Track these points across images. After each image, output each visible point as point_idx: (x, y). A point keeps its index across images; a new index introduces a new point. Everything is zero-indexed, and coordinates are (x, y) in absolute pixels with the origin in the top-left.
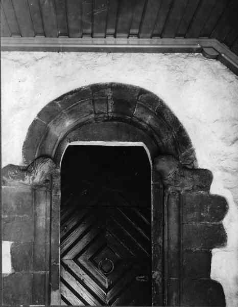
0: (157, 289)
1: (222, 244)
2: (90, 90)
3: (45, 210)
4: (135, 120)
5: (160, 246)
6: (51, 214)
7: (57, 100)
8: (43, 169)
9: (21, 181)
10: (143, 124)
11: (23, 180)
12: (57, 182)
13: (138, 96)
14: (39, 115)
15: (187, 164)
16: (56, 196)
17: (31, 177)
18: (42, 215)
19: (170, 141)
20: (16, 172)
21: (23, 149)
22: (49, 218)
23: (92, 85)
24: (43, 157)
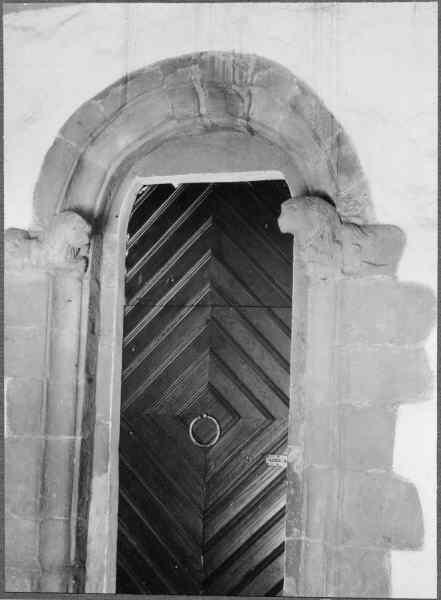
1: (420, 396)
2: (160, 72)
7: (96, 98)
10: (271, 134)
14: (63, 131)
17: (44, 252)
19: (322, 167)
23: (164, 61)
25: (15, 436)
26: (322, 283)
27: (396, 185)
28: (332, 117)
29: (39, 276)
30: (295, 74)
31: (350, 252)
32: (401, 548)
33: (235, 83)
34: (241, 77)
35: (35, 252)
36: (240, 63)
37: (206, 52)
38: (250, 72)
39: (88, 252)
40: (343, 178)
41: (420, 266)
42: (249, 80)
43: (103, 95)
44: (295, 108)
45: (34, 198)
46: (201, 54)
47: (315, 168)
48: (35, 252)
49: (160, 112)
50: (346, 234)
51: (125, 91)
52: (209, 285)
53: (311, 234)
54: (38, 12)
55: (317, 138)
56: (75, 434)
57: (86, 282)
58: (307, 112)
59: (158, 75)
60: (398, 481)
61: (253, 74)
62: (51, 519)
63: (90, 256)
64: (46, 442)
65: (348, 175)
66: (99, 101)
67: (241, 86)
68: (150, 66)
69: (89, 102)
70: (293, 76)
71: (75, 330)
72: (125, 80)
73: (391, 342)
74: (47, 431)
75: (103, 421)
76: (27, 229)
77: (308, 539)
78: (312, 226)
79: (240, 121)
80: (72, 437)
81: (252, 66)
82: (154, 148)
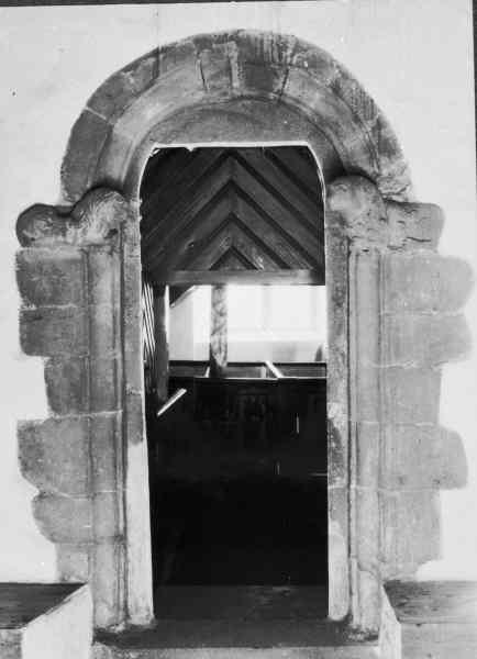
0: (338, 440)
3: (110, 292)
4: (288, 101)
5: (343, 355)
6: (122, 293)
7: (126, 69)
8: (104, 212)
9: (60, 238)
10: (304, 109)
11: (64, 235)
12: (134, 230)
13: (292, 56)
14: (91, 103)
15: (394, 194)
16: (131, 256)
17: (80, 231)
18: (106, 301)
20: (50, 220)
21: (62, 172)
22: (118, 306)
24: (104, 186)
26: (364, 254)
27: (433, 154)
28: (372, 101)
30: (335, 58)
31: (396, 229)
32: (448, 487)
33: (273, 61)
34: (280, 57)
35: (71, 231)
36: (280, 45)
37: (242, 30)
38: (289, 52)
40: (384, 160)
41: (458, 240)
42: (289, 60)
43: (133, 67)
44: (336, 89)
46: (238, 31)
47: (352, 143)
48: (71, 231)
49: (190, 86)
50: (394, 214)
51: (157, 64)
52: (254, 250)
53: (359, 212)
55: (357, 119)
58: (346, 94)
59: (191, 50)
60: (443, 432)
61: (292, 56)
62: (100, 493)
65: (389, 157)
66: (129, 73)
67: (279, 65)
68: (183, 40)
69: (119, 73)
70: (332, 60)
72: (156, 53)
73: (435, 309)
75: (134, 391)
77: (358, 488)
78: (359, 206)
79: (272, 96)
81: (291, 46)
82: (184, 119)
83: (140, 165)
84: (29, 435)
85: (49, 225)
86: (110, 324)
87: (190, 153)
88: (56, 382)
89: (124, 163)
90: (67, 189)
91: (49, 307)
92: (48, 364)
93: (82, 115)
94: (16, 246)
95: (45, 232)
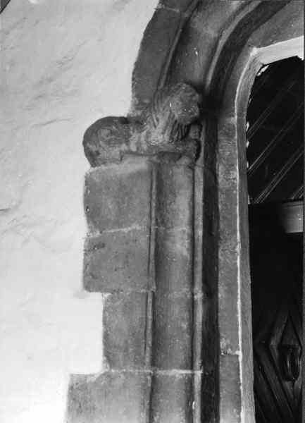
9: (124, 147)
17: (144, 133)
25: (113, 371)
29: (142, 164)
39: (200, 135)
45: (133, 79)
54: (188, 225)
56: (192, 368)
57: (199, 172)
63: (202, 139)
64: (154, 378)
71: (187, 229)
74: (154, 363)
75: (229, 351)
76: (126, 116)
80: (189, 372)
83: (243, 69)
84: (80, 394)
85: (112, 133)
86: (186, 253)
87: (255, 45)
88: (114, 326)
89: (167, 58)
90: (137, 96)
91: (112, 231)
92: (107, 301)
93: (155, 13)
94: (86, 166)
95: (109, 143)
